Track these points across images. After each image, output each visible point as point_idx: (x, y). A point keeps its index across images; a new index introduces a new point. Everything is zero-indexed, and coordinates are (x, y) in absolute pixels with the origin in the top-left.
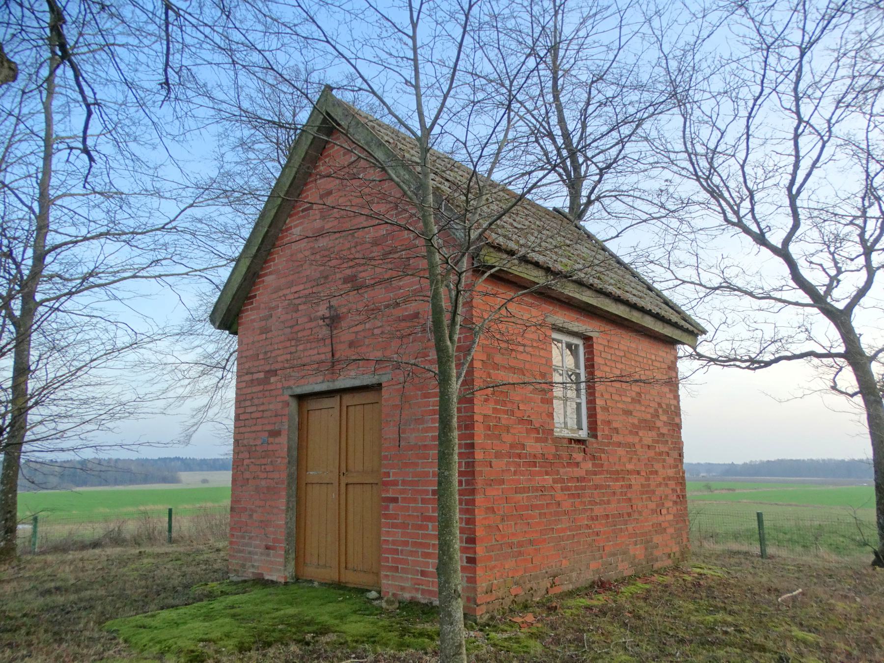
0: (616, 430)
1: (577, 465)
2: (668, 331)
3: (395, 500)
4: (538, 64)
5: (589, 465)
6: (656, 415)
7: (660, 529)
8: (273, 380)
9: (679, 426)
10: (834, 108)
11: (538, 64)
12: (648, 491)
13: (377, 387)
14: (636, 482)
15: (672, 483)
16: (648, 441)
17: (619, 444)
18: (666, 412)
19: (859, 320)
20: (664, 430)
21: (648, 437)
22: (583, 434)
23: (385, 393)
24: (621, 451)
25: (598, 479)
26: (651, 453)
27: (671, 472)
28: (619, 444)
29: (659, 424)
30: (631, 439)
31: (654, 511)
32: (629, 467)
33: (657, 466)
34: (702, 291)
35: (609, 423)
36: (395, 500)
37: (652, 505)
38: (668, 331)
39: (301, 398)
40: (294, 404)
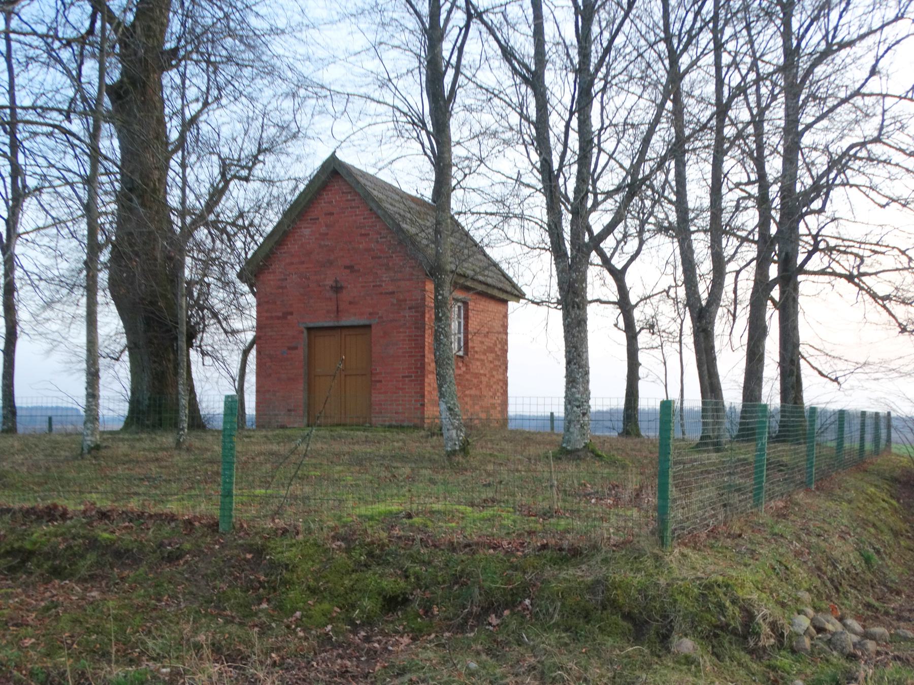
0: (477, 352)
1: (460, 368)
2: (504, 296)
3: (380, 381)
4: (461, 187)
5: (464, 369)
6: (495, 345)
7: (493, 406)
8: (289, 317)
9: (506, 351)
10: (616, 143)
11: (461, 187)
12: (489, 386)
13: (368, 327)
14: (484, 380)
15: (501, 384)
16: (490, 359)
17: (477, 360)
18: (500, 342)
19: (630, 279)
20: (499, 353)
21: (491, 356)
22: (461, 353)
23: (373, 328)
24: (478, 363)
25: (468, 376)
26: (492, 366)
27: (501, 377)
28: (477, 360)
29: (497, 349)
30: (482, 357)
31: (491, 397)
32: (482, 372)
33: (494, 373)
34: (526, 250)
35: (474, 347)
36: (380, 381)
37: (491, 394)
38: (504, 296)
39: (309, 329)
40: (305, 331)
